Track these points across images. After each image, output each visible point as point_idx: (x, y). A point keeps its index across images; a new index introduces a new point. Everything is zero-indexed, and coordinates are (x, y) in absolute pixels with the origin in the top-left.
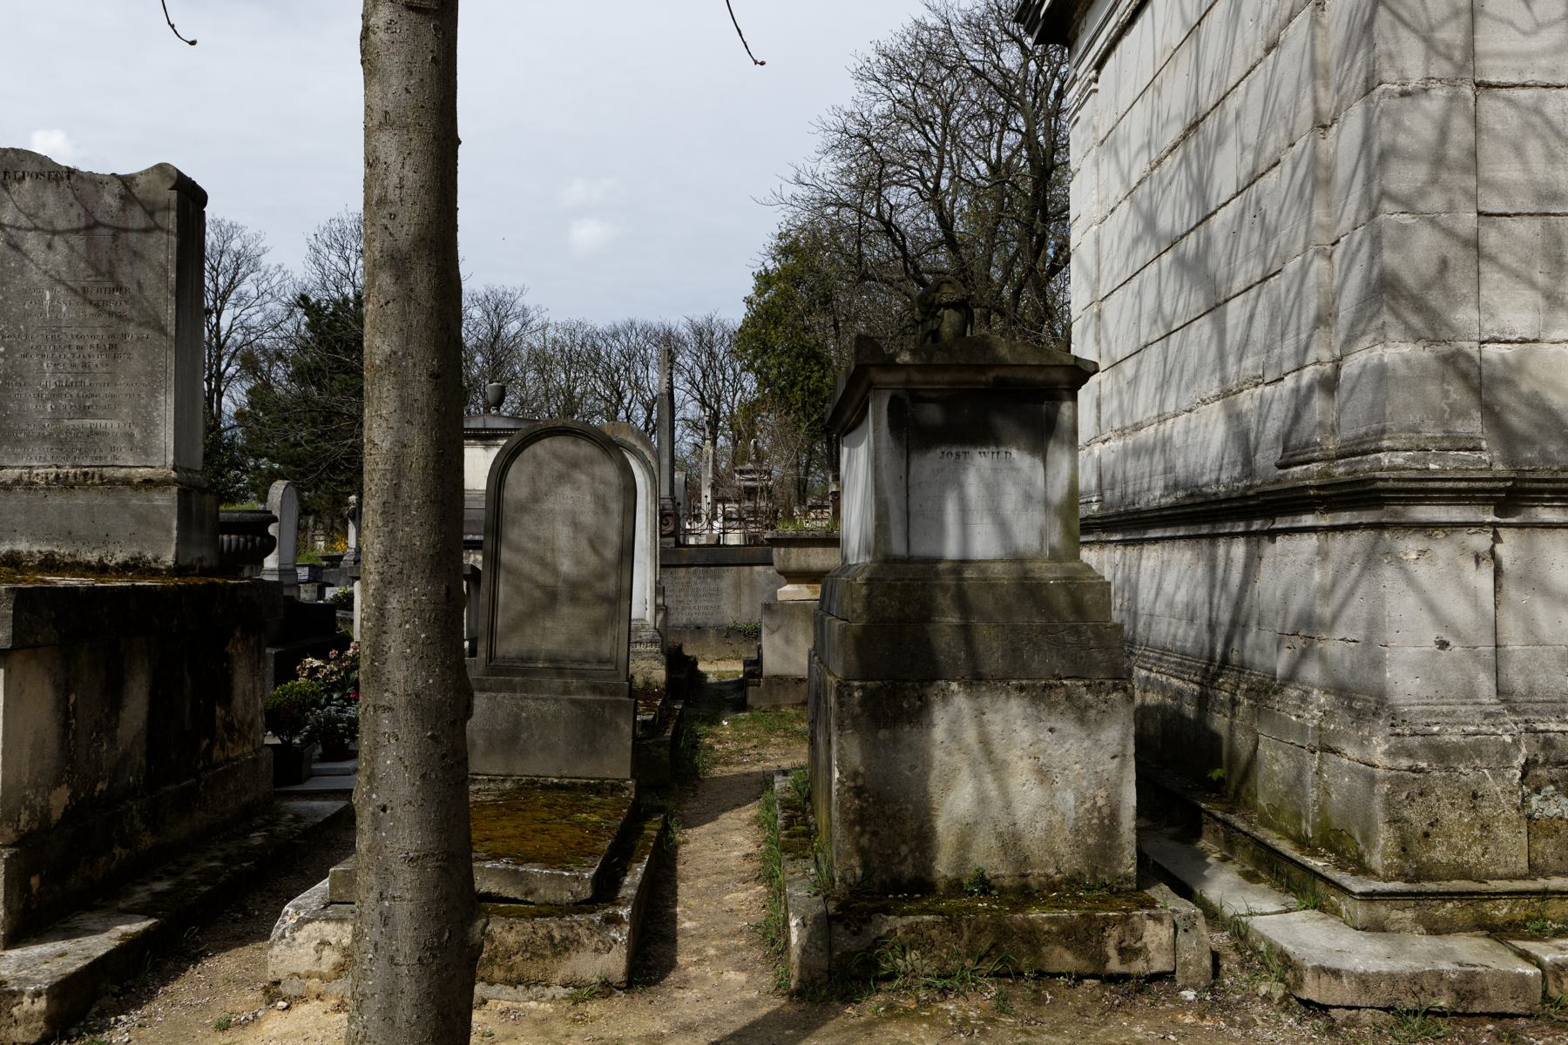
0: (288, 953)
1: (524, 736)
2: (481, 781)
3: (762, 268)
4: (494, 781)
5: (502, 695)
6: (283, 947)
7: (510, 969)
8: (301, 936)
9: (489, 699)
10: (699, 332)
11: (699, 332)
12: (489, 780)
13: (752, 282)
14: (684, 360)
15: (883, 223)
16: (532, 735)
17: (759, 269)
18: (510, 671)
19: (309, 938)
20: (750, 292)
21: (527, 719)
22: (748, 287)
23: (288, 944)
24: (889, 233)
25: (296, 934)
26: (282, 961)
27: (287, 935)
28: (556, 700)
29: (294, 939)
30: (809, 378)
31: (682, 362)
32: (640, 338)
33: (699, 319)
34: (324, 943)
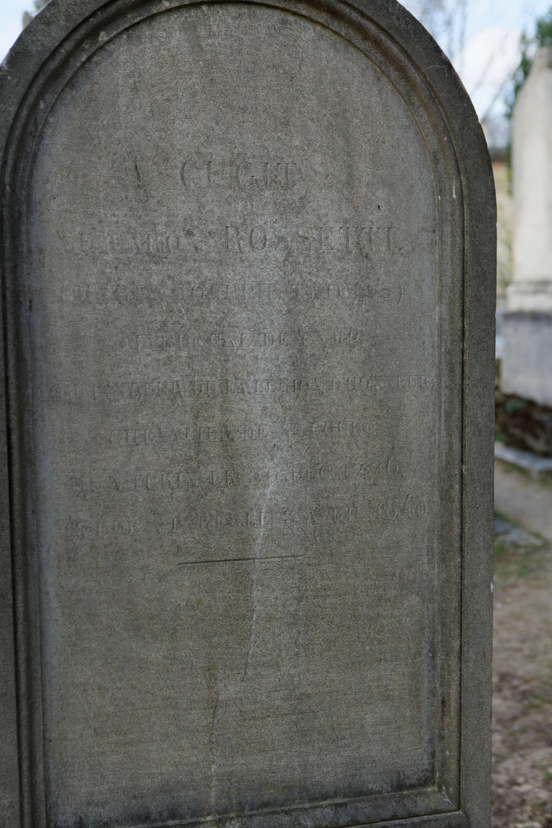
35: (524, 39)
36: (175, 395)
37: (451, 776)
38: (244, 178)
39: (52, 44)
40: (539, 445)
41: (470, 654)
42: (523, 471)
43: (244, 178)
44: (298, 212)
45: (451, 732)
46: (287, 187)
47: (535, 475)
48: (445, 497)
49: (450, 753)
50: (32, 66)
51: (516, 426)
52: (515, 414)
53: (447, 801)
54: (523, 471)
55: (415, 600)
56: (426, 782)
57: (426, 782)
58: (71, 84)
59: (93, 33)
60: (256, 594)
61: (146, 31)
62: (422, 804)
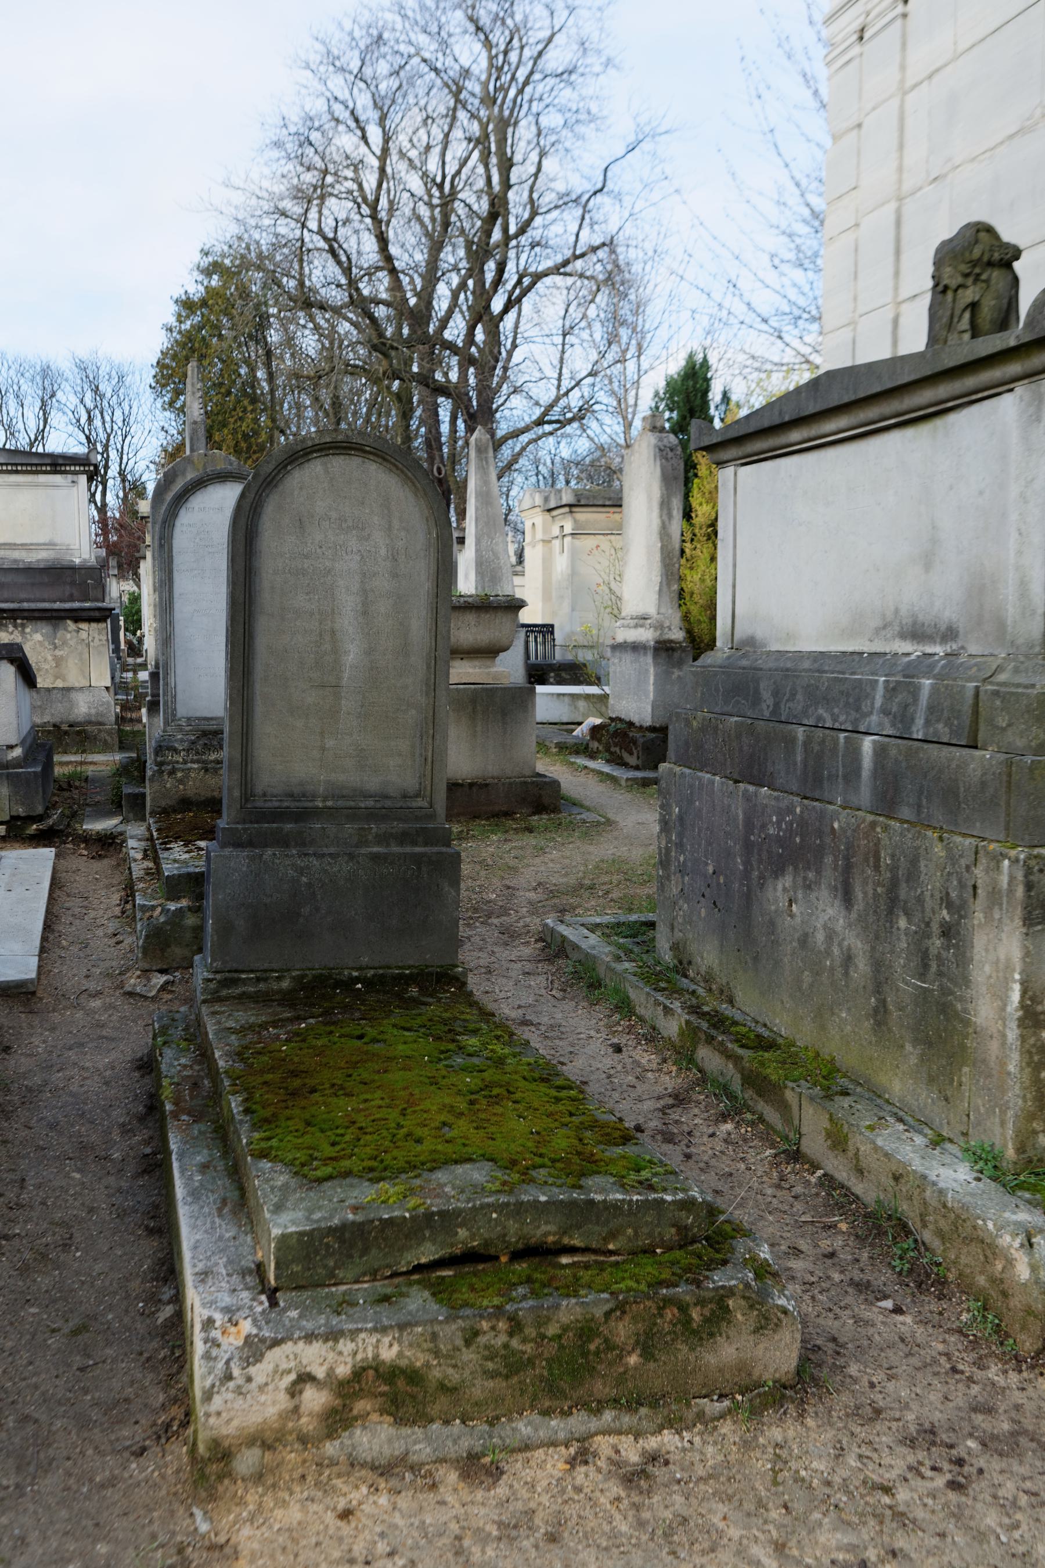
0: (239, 1403)
1: (306, 910)
2: (244, 982)
3: (182, 292)
4: (266, 980)
5: (269, 852)
6: (230, 1396)
7: (621, 1380)
8: (260, 1372)
9: (252, 859)
10: (82, 367)
11: (82, 367)
12: (258, 980)
13: (173, 308)
14: (67, 397)
15: (325, 239)
16: (317, 909)
17: (178, 293)
18: (279, 815)
19: (279, 1373)
20: (172, 320)
21: (309, 885)
22: (168, 313)
23: (239, 1391)
24: (332, 252)
25: (252, 1370)
26: (229, 1421)
27: (236, 1372)
28: (351, 857)
29: (249, 1379)
30: (241, 419)
31: (63, 400)
32: (12, 372)
33: (83, 353)
34: (305, 1378)
35: (657, 394)
36: (312, 614)
37: (428, 793)
38: (344, 525)
39: (269, 471)
40: (632, 760)
41: (437, 737)
42: (614, 780)
43: (344, 525)
44: (367, 540)
45: (428, 773)
46: (363, 529)
47: (623, 783)
48: (428, 667)
49: (428, 783)
50: (261, 479)
51: (616, 745)
52: (616, 734)
53: (426, 805)
54: (614, 780)
55: (414, 712)
56: (417, 795)
57: (417, 795)
58: (276, 486)
59: (286, 466)
60: (343, 702)
61: (306, 465)
62: (414, 804)
